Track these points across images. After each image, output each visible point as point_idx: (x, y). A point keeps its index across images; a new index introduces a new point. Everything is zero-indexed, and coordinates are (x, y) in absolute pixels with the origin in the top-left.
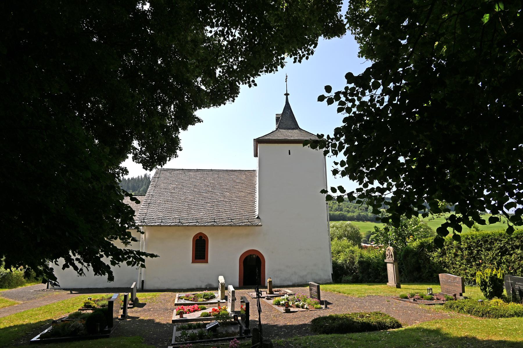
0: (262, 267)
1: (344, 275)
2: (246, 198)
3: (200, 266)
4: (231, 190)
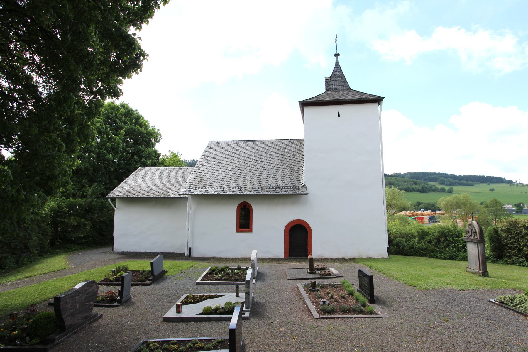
3: (244, 236)
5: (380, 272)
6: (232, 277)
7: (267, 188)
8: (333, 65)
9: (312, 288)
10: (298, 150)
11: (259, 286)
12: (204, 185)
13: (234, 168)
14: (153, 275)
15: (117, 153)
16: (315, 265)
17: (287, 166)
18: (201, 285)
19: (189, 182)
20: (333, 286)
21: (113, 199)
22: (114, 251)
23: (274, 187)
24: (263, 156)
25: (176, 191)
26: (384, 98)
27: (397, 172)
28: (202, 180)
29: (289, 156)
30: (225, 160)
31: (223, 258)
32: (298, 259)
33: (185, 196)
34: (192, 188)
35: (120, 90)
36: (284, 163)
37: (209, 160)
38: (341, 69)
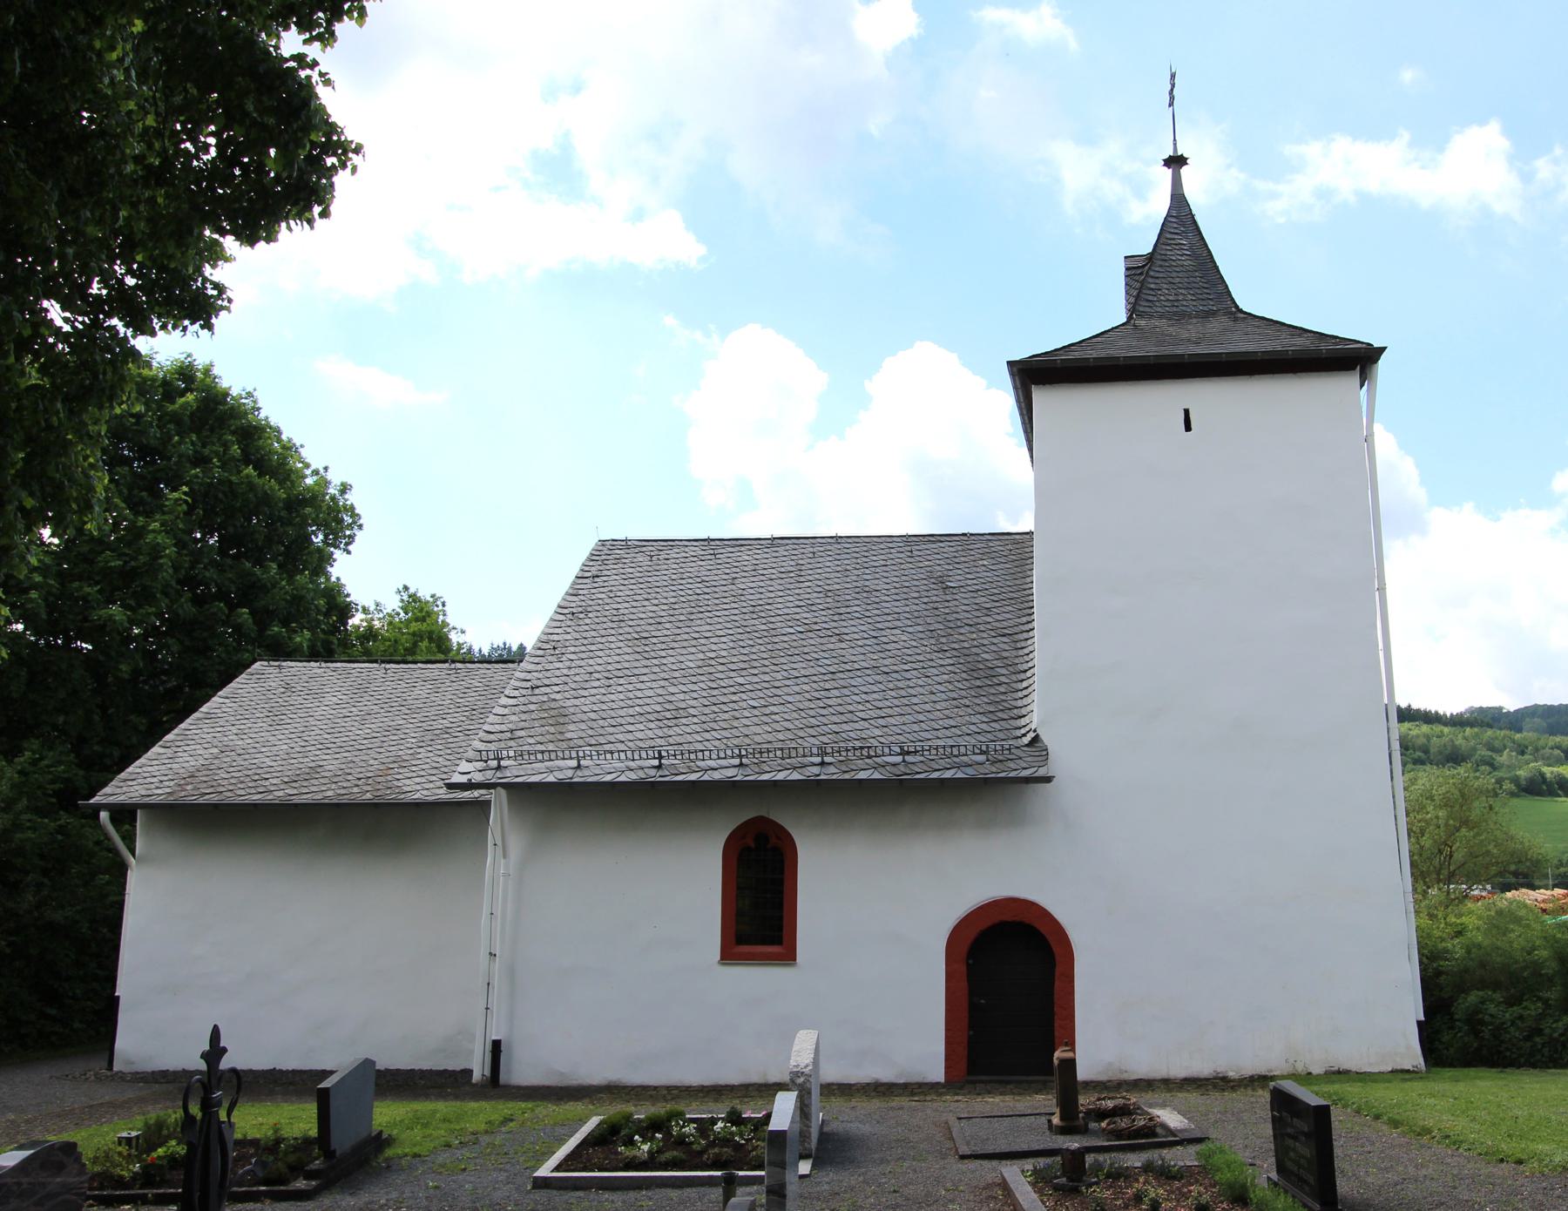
5: (1377, 1117)
6: (701, 1153)
7: (865, 752)
8: (1160, 206)
9: (1070, 1179)
10: (1008, 583)
11: (826, 1187)
12: (572, 744)
13: (713, 663)
14: (328, 1154)
15: (146, 597)
16: (1085, 1101)
17: (955, 653)
18: (555, 1192)
19: (498, 728)
20: (1165, 1174)
21: (124, 815)
22: (115, 1069)
23: (898, 750)
24: (848, 610)
25: (434, 772)
26: (1386, 348)
27: (1485, 705)
28: (561, 721)
29: (964, 608)
30: (668, 626)
31: (655, 1088)
32: (1011, 1086)
33: (476, 793)
34: (512, 754)
35: (217, 286)
36: (944, 640)
37: (593, 627)
38: (1195, 222)
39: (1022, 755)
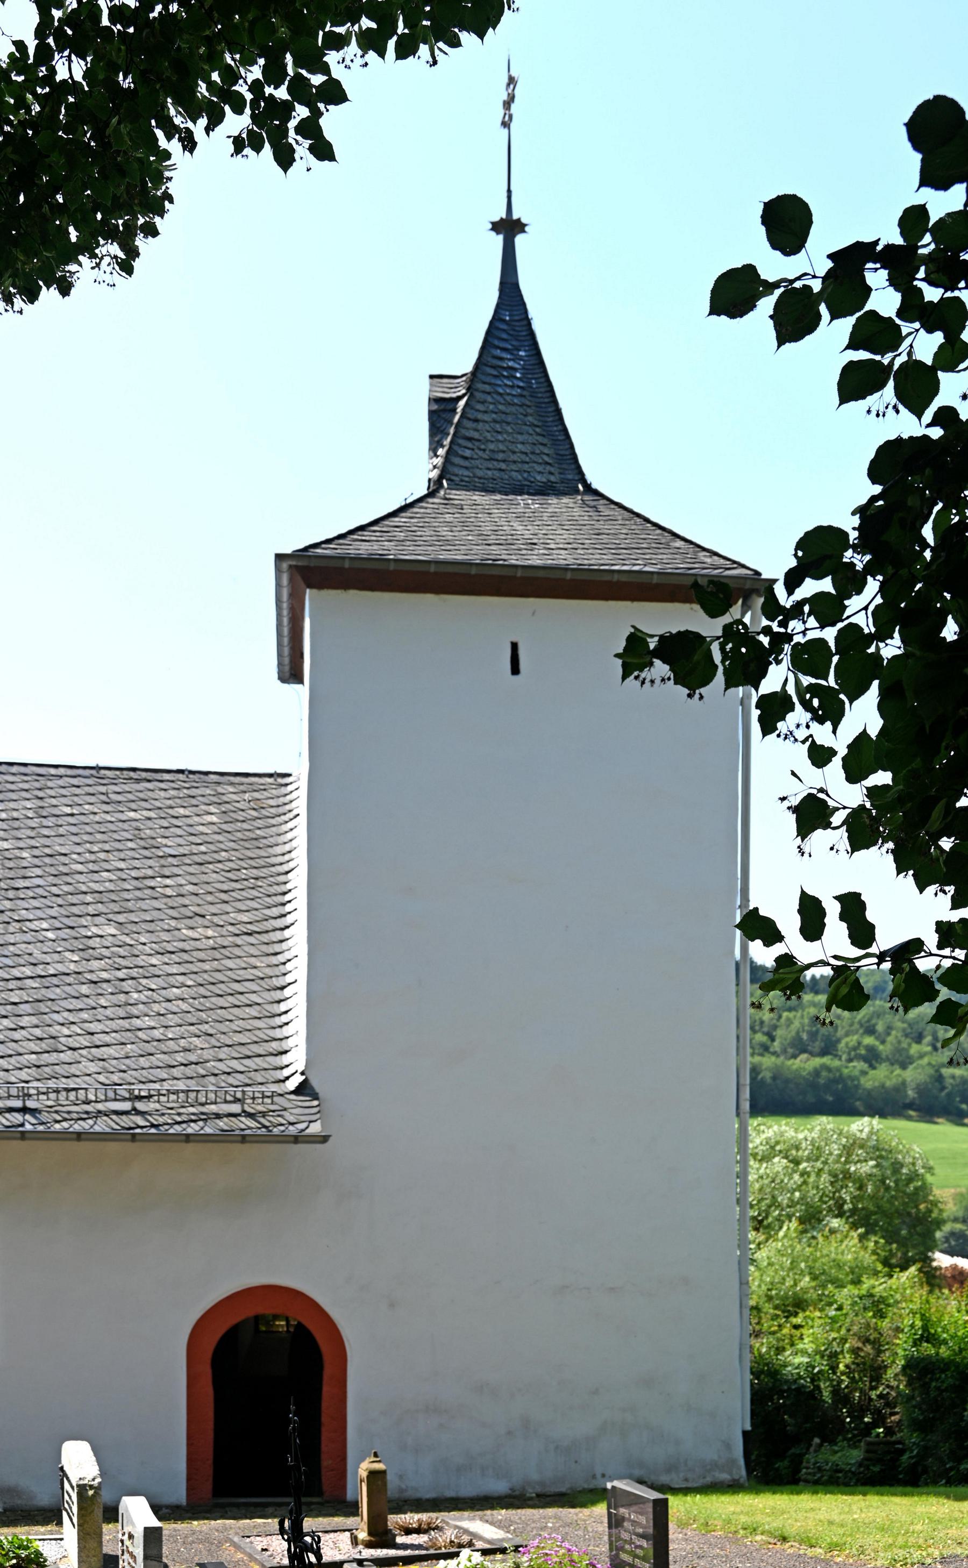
0: (327, 1390)
1: (817, 1440)
2: (230, 964)
4: (130, 905)
24: (27, 883)
39: (287, 1105)
